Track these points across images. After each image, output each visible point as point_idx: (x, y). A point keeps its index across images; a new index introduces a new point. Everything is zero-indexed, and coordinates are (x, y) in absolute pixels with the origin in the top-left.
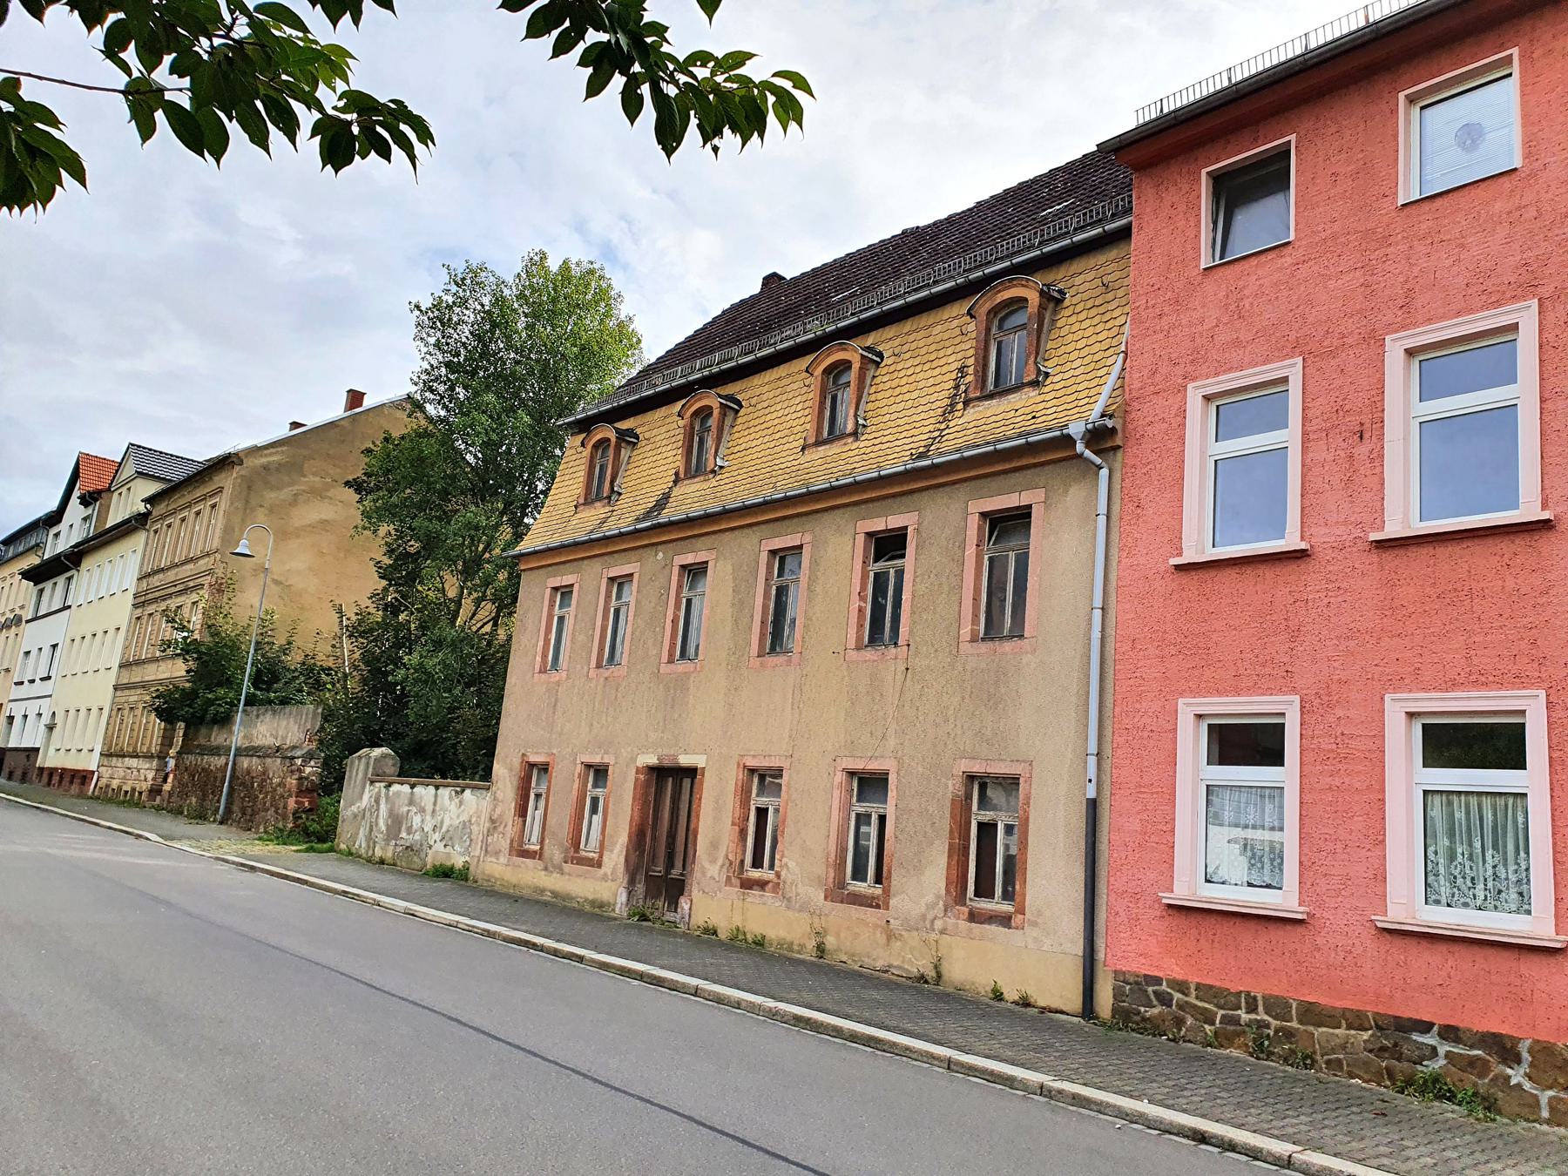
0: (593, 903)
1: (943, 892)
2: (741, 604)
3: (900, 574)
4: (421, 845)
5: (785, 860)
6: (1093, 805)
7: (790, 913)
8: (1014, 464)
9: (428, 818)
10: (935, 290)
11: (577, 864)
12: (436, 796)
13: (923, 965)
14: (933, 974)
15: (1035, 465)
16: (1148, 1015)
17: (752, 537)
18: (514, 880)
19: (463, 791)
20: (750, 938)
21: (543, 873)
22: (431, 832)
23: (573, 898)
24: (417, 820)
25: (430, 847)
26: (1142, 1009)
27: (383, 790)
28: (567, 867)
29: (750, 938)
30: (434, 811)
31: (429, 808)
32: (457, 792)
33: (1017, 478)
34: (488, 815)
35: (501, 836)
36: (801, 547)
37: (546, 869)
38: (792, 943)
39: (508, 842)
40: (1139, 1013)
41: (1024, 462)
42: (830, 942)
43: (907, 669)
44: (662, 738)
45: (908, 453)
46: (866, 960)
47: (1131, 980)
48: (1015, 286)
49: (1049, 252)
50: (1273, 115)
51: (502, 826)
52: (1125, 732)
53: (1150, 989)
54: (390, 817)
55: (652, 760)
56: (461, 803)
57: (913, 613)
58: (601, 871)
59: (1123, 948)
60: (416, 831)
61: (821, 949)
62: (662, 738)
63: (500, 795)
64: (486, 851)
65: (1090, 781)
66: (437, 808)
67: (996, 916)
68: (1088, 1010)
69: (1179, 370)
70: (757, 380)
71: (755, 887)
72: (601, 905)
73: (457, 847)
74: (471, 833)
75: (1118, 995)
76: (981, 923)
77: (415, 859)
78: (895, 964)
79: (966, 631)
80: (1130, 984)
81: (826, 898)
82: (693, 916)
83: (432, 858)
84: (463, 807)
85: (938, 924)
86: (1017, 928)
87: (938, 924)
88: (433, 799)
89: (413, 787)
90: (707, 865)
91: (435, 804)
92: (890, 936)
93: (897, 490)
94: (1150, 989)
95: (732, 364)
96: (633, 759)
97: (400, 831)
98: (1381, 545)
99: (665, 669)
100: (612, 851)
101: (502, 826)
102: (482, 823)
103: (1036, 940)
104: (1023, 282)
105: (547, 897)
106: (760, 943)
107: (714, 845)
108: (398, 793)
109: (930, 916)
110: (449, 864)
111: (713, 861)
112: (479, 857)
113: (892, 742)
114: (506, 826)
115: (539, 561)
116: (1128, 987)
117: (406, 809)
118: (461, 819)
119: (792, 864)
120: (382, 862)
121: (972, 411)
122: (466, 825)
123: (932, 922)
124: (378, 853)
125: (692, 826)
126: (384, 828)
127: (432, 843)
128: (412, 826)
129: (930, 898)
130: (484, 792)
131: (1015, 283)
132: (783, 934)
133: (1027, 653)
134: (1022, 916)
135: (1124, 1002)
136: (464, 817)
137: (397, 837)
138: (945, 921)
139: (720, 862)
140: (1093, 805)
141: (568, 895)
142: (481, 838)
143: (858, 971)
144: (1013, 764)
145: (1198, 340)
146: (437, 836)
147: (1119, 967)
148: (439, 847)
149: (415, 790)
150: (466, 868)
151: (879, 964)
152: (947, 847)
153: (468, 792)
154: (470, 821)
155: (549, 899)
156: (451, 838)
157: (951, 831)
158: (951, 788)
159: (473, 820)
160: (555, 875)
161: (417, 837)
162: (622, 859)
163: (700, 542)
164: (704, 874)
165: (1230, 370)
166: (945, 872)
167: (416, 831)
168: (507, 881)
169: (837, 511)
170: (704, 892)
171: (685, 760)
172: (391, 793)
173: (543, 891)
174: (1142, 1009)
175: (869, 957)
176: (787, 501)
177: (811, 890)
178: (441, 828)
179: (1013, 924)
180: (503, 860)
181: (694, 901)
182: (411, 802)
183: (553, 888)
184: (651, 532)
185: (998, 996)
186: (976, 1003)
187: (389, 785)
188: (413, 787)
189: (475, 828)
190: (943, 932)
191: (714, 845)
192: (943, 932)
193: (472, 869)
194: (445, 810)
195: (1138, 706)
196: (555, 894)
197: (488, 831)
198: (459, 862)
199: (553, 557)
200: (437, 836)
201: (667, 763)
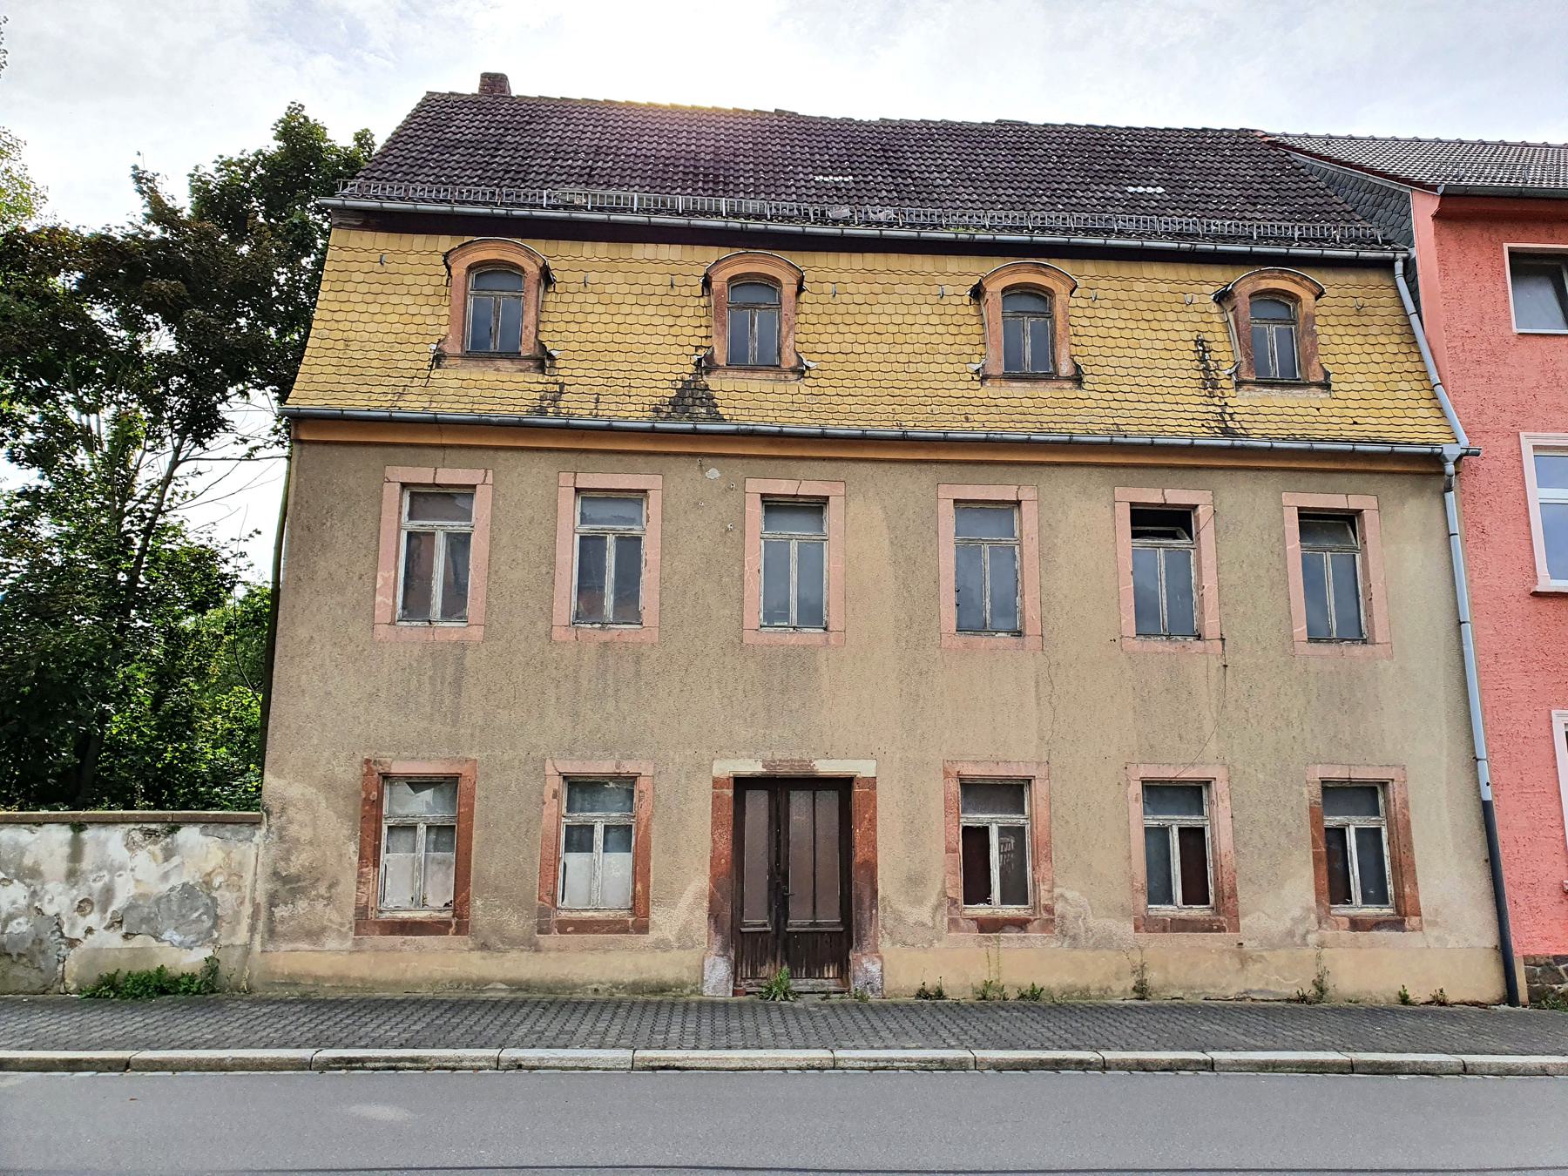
1: (1314, 904)
3: (459, 544)
5: (1057, 891)
6: (1486, 807)
7: (1077, 953)
8: (1294, 465)
10: (459, 209)
13: (1297, 983)
14: (1314, 991)
15: (744, 456)
16: (1561, 990)
17: (926, 476)
20: (1013, 995)
23: (575, 986)
26: (1556, 987)
28: (545, 940)
29: (1013, 995)
33: (1342, 480)
35: (320, 905)
36: (1018, 503)
37: (484, 946)
38: (1088, 989)
40: (1553, 990)
41: (1348, 466)
42: (1154, 978)
43: (1225, 666)
45: (890, 409)
46: (1212, 990)
47: (1542, 962)
48: (1284, 279)
49: (498, 214)
50: (1544, 221)
52: (1499, 738)
53: (1561, 968)
57: (1222, 604)
59: (1528, 934)
61: (1141, 991)
65: (1488, 784)
66: (86, 864)
67: (1384, 922)
68: (1511, 997)
69: (1507, 417)
70: (588, 249)
71: (1007, 929)
75: (1531, 979)
76: (1369, 930)
78: (1255, 988)
80: (1541, 966)
81: (1137, 929)
82: (886, 978)
83: (74, 967)
85: (1312, 938)
86: (1414, 930)
87: (1312, 938)
90: (904, 908)
92: (1244, 959)
93: (1150, 461)
94: (1561, 968)
95: (759, 226)
98: (1536, 594)
101: (326, 884)
103: (1437, 939)
104: (1297, 279)
106: (1033, 995)
109: (1301, 930)
113: (1213, 747)
116: (1538, 969)
121: (1247, 394)
123: (1304, 937)
125: (860, 855)
129: (1297, 912)
131: (1285, 275)
133: (1382, 658)
134: (1418, 918)
135: (1536, 983)
138: (1320, 934)
139: (933, 900)
140: (1486, 807)
142: (247, 910)
143: (1203, 1004)
144: (1384, 769)
145: (1521, 396)
147: (1526, 953)
150: (212, 967)
151: (1231, 993)
152: (1311, 857)
157: (1314, 840)
158: (1306, 795)
162: (702, 914)
165: (1556, 429)
166: (1312, 883)
169: (1177, 472)
170: (904, 943)
174: (1556, 987)
175: (1215, 987)
179: (1407, 927)
180: (332, 943)
181: (885, 957)
185: (1404, 1000)
190: (1322, 945)
192: (1322, 945)
193: (224, 970)
195: (1508, 714)
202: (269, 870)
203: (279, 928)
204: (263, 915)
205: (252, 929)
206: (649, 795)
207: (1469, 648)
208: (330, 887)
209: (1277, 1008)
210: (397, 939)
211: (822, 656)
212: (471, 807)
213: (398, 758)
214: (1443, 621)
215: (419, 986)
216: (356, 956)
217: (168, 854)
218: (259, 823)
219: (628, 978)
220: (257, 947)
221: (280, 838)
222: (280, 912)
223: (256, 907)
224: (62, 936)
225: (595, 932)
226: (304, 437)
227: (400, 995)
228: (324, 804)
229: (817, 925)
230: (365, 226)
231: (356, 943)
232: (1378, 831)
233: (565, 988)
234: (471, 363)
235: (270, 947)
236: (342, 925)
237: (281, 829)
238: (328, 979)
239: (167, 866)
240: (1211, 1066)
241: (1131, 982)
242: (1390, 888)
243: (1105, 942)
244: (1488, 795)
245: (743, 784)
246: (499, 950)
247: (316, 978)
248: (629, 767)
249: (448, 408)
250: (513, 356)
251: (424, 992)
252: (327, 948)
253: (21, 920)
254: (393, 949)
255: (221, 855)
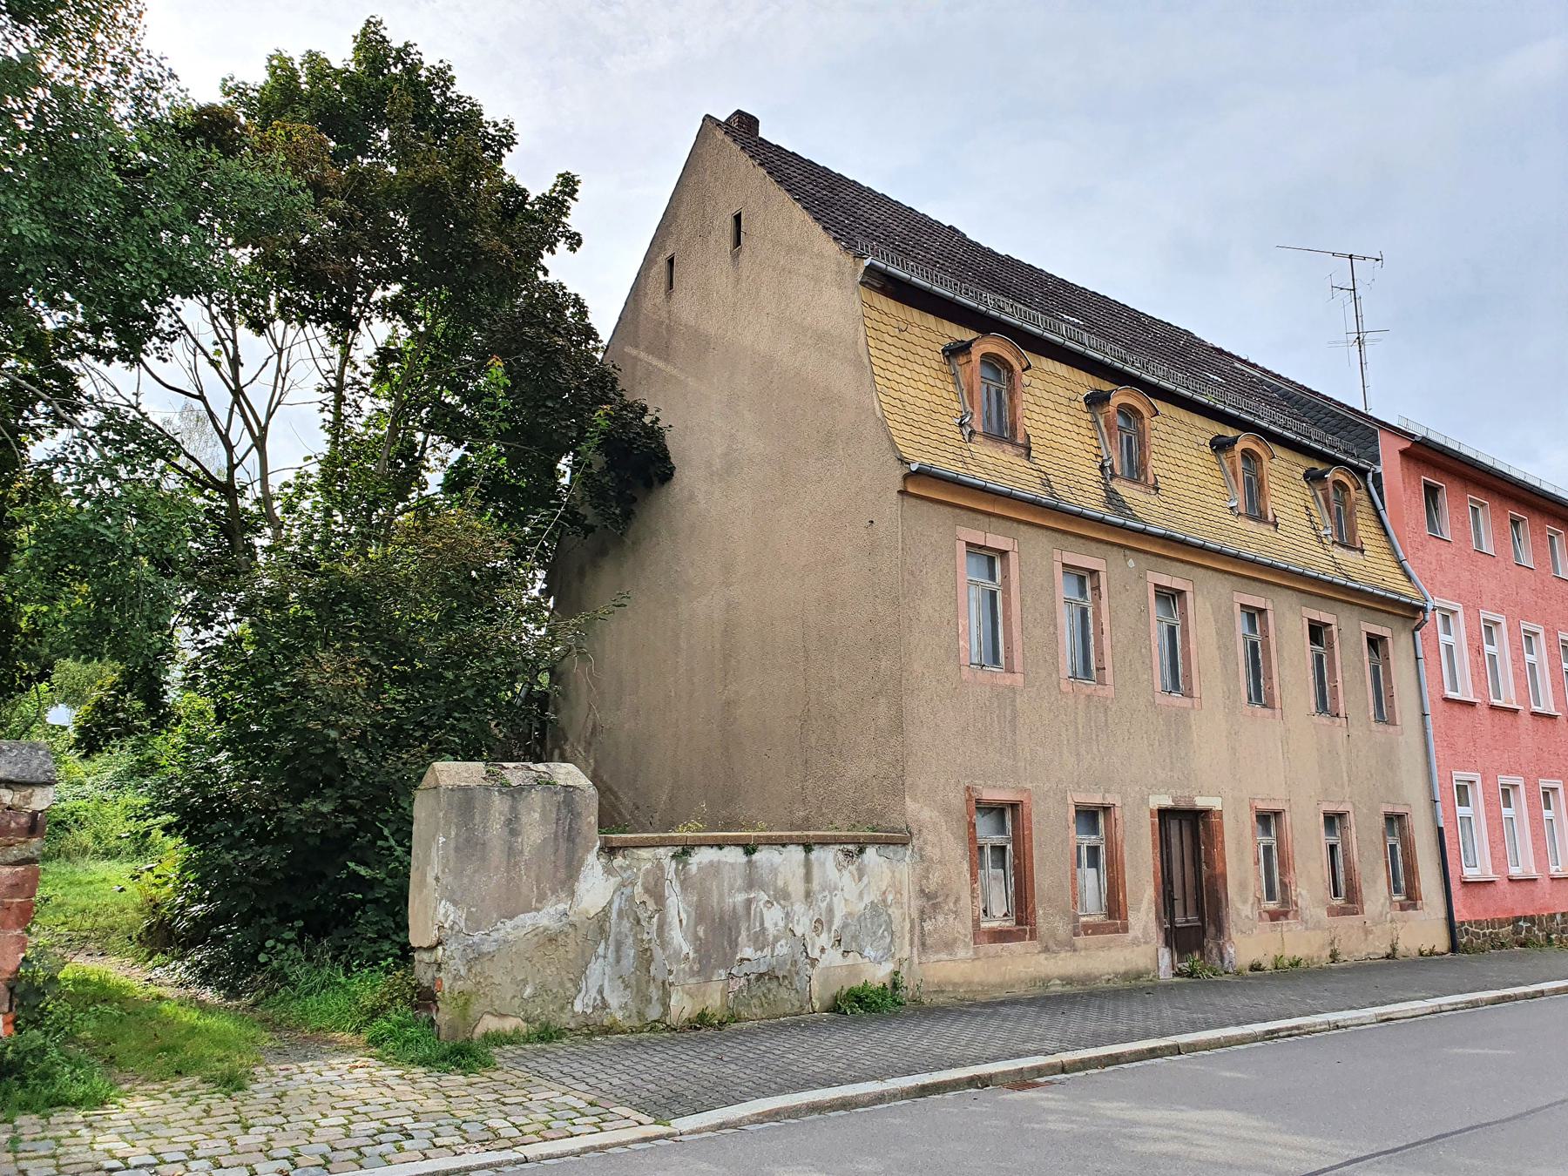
0: (1126, 976)
2: (1225, 648)
4: (794, 963)
9: (799, 907)
11: (1092, 934)
12: (808, 864)
18: (993, 978)
19: (861, 851)
21: (1043, 956)
22: (810, 935)
23: (1096, 978)
24: (773, 918)
25: (814, 962)
27: (670, 867)
28: (1080, 941)
30: (808, 894)
31: (797, 888)
32: (848, 854)
34: (914, 889)
35: (951, 917)
37: (1046, 949)
39: (970, 924)
44: (1172, 777)
51: (952, 900)
54: (700, 919)
55: (1167, 802)
56: (861, 873)
58: (1131, 934)
60: (776, 939)
62: (1172, 777)
63: (932, 852)
64: (923, 944)
66: (815, 886)
72: (1138, 976)
73: (868, 951)
74: (890, 922)
77: (784, 993)
79: (1158, 687)
83: (819, 990)
84: (865, 879)
88: (801, 871)
89: (749, 850)
90: (1239, 905)
91: (808, 877)
92: (1367, 932)
96: (1145, 801)
97: (734, 945)
99: (1162, 699)
100: (1138, 910)
102: (905, 899)
105: (1056, 988)
107: (1243, 886)
108: (714, 869)
110: (857, 984)
111: (1245, 902)
112: (910, 959)
114: (957, 901)
115: (1035, 515)
117: (740, 898)
118: (867, 900)
119: (1304, 892)
120: (701, 1021)
122: (876, 909)
124: (682, 1006)
126: (687, 948)
127: (815, 954)
128: (763, 929)
130: (900, 849)
132: (1306, 952)
136: (872, 896)
137: (728, 959)
140: (1440, 830)
141: (1088, 975)
142: (907, 926)
146: (824, 939)
148: (833, 958)
149: (756, 856)
153: (871, 852)
154: (884, 901)
155: (1060, 989)
156: (854, 938)
159: (890, 898)
160: (1063, 955)
161: (782, 949)
162: (1152, 915)
163: (1338, 607)
164: (1239, 915)
167: (776, 939)
168: (981, 984)
171: (1201, 802)
172: (693, 869)
173: (1046, 981)
176: (1253, 563)
177: (1318, 910)
178: (830, 922)
180: (961, 953)
182: (752, 881)
183: (1062, 972)
184: (1160, 541)
186: (1415, 962)
187: (685, 851)
188: (749, 850)
189: (895, 912)
191: (1243, 886)
194: (833, 889)
196: (1068, 980)
197: (922, 912)
198: (878, 974)
199: (953, 494)
200: (824, 939)
201: (1183, 805)
202: (918, 888)
203: (929, 941)
204: (917, 928)
205: (911, 944)
206: (1119, 822)
207: (1431, 731)
208: (955, 903)
209: (1382, 965)
210: (998, 946)
211: (1192, 713)
212: (1031, 829)
213: (986, 786)
214: (1417, 714)
215: (1013, 986)
216: (976, 962)
217: (861, 873)
218: (904, 844)
219: (1122, 969)
220: (916, 960)
221: (921, 857)
222: (928, 926)
223: (912, 922)
224: (807, 957)
225: (1102, 933)
226: (910, 490)
227: (1002, 995)
228: (944, 827)
229: (1187, 921)
230: (883, 291)
231: (976, 952)
232: (1004, 848)
233: (1091, 980)
234: (989, 442)
235: (924, 959)
236: (966, 936)
237: (921, 849)
238: (961, 985)
239: (862, 885)
240: (1542, 993)
241: (1328, 952)
242: (1403, 883)
243: (1318, 926)
244: (1442, 825)
245: (1164, 814)
246: (1054, 952)
247: (955, 985)
248: (1109, 800)
249: (979, 477)
250: (1013, 443)
251: (1019, 991)
252: (959, 956)
253: (783, 942)
254: (997, 956)
255: (887, 874)
